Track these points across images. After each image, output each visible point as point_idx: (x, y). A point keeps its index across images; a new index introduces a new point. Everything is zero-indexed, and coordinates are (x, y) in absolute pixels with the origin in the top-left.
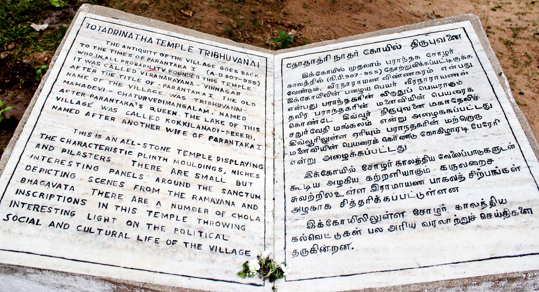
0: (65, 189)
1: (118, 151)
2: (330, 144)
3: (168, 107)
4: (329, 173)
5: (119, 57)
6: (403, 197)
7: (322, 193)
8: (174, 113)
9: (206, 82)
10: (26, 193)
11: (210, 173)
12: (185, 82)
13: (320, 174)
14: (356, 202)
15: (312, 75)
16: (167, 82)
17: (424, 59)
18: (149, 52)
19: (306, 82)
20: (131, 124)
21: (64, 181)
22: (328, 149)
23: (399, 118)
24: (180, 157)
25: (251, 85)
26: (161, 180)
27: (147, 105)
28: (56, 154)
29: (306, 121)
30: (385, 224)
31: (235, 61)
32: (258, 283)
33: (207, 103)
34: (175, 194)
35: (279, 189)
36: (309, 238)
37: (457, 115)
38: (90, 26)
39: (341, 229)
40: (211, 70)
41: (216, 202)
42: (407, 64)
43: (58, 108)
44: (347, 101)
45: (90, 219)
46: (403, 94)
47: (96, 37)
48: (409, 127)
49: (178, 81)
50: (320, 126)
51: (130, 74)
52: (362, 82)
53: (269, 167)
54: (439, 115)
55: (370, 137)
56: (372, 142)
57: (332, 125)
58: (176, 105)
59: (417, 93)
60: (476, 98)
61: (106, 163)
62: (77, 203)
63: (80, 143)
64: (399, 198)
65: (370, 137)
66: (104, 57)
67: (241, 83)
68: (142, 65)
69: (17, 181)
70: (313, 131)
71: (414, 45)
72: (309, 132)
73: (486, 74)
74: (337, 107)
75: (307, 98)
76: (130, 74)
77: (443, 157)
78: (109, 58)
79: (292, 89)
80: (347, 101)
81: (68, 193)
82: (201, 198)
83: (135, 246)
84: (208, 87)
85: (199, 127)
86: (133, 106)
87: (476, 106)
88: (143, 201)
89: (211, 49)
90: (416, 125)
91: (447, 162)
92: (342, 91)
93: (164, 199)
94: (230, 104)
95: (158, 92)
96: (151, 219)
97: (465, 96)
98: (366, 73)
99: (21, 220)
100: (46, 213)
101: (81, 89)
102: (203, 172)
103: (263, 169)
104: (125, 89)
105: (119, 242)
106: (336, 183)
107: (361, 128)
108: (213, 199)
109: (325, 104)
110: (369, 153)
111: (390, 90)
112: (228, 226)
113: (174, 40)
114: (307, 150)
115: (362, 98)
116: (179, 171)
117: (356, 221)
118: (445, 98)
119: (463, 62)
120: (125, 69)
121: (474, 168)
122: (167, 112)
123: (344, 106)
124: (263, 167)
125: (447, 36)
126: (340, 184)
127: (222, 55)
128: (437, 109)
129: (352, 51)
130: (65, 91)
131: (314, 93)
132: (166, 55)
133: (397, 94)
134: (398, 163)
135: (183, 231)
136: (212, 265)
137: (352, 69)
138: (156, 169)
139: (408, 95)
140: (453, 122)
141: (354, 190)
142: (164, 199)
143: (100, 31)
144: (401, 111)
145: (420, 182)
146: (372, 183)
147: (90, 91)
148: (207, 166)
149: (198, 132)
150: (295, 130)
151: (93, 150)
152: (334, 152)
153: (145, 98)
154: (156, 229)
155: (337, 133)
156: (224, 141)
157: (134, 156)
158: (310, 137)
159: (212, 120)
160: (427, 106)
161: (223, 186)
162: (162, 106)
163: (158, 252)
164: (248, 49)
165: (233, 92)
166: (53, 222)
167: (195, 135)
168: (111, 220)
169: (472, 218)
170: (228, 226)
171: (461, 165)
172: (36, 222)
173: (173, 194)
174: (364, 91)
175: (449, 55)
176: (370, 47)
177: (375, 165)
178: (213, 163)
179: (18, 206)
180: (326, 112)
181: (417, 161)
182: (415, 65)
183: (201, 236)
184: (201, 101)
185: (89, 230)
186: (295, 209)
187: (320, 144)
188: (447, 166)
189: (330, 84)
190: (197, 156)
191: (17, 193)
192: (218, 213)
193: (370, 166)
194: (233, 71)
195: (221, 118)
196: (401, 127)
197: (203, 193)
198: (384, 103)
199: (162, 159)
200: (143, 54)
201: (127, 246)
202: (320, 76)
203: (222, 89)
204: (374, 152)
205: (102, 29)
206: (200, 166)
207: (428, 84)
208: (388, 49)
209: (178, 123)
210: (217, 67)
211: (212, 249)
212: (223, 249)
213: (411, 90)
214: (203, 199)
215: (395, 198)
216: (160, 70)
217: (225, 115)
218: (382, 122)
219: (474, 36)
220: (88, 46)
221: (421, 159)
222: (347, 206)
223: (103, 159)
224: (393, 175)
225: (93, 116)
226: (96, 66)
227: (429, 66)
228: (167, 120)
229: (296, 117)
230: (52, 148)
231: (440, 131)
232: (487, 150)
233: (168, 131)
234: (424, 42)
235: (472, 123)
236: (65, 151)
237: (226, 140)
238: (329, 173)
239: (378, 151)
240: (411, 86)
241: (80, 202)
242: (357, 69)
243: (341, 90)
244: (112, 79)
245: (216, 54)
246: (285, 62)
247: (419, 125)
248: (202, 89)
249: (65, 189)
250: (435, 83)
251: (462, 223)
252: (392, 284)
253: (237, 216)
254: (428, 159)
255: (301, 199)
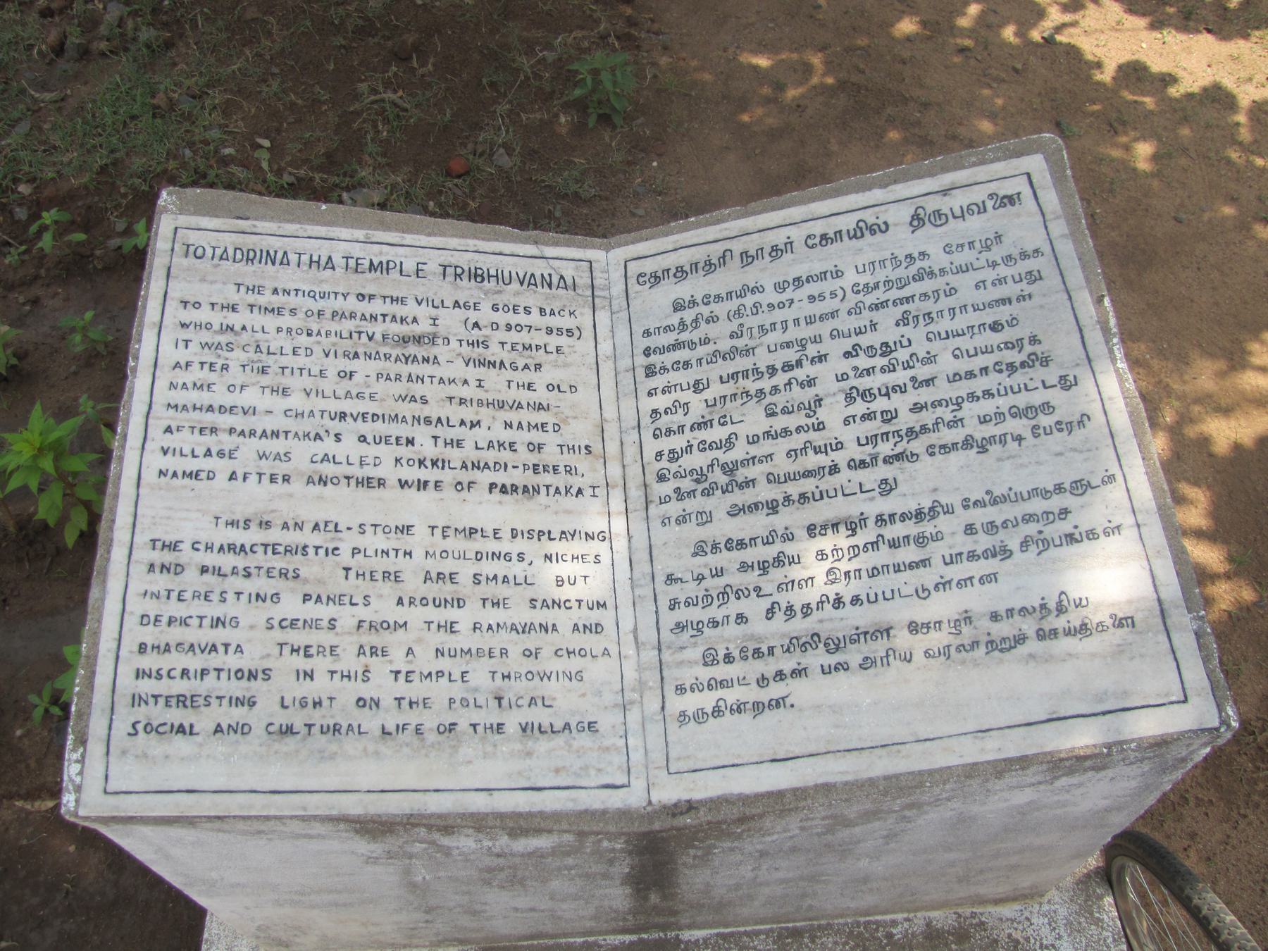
0: (226, 652)
1: (311, 551)
2: (741, 474)
3: (395, 430)
4: (741, 544)
5: (271, 322)
6: (888, 595)
7: (728, 589)
8: (410, 442)
9: (466, 350)
10: (154, 674)
11: (498, 567)
12: (420, 359)
13: (722, 546)
14: (797, 608)
15: (693, 303)
16: (380, 365)
17: (938, 259)
18: (332, 296)
19: (682, 323)
20: (325, 484)
21: (220, 635)
22: (736, 489)
23: (882, 413)
24: (439, 543)
25: (563, 341)
26: (406, 601)
27: (350, 429)
28: (191, 580)
29: (688, 421)
30: (853, 656)
31: (522, 284)
32: (618, 783)
33: (475, 404)
34: (439, 626)
35: (642, 582)
36: (709, 685)
37: (1003, 403)
38: (192, 249)
39: (768, 667)
40: (473, 316)
41: (520, 630)
42: (901, 272)
43: (170, 473)
44: (772, 370)
45: (287, 707)
46: (891, 351)
47: (210, 278)
48: (903, 433)
49: (407, 359)
50: (716, 433)
51: (301, 361)
52: (802, 322)
53: (618, 535)
54: (966, 405)
55: (822, 460)
56: (827, 470)
57: (743, 430)
58: (409, 420)
59: (921, 349)
60: (1045, 362)
61: (291, 584)
62: (255, 678)
63: (232, 548)
64: (880, 597)
65: (822, 460)
66: (238, 328)
67: (539, 338)
68: (323, 333)
69: (131, 652)
70: (704, 447)
71: (917, 221)
72: (695, 448)
73: (1070, 298)
74: (752, 385)
75: (687, 364)
76: (301, 361)
77: (971, 504)
78: (249, 328)
79: (653, 342)
80: (772, 370)
81: (233, 661)
82: (490, 627)
83: (382, 748)
84: (471, 363)
85: (464, 466)
86: (321, 439)
87: (1043, 382)
88: (379, 653)
89: (464, 260)
90: (917, 429)
91: (979, 516)
92: (761, 345)
93: (419, 641)
94: (524, 396)
95: (367, 396)
96: (402, 688)
97: (1023, 357)
98: (812, 298)
99: (161, 729)
100: (203, 708)
101: (208, 419)
102: (488, 568)
103: (607, 542)
104: (296, 401)
105: (351, 744)
106: (756, 565)
107: (803, 437)
108: (505, 576)
109: (725, 379)
110: (822, 498)
111: (865, 341)
112: (549, 678)
113: (381, 253)
114: (694, 491)
115: (804, 362)
116: (439, 574)
117: (798, 650)
118: (981, 361)
119: (1024, 266)
120: (288, 349)
121: (1031, 529)
122: (393, 440)
123: (766, 384)
124: (607, 535)
125: (991, 196)
126: (764, 567)
127: (493, 272)
128: (963, 388)
129: (779, 237)
130: (174, 428)
131: (702, 351)
132: (371, 297)
133: (879, 352)
134: (880, 520)
135: (464, 703)
136: (528, 761)
137: (780, 287)
138: (392, 577)
139: (902, 354)
140: (994, 421)
141: (793, 581)
142: (419, 641)
143: (216, 261)
144: (887, 394)
145: (924, 563)
146: (827, 565)
147: (225, 421)
148: (493, 553)
149: (465, 477)
150: (666, 444)
151: (260, 558)
152: (748, 496)
153: (343, 416)
154: (414, 706)
155: (754, 450)
156: (520, 491)
157: (345, 557)
158: (697, 460)
159: (490, 445)
160: (941, 382)
161: (530, 593)
162: (381, 428)
163: (424, 752)
164: (547, 245)
165: (526, 367)
166: (219, 725)
167: (459, 487)
168: (326, 703)
169: (1020, 639)
170: (549, 678)
171: (1005, 522)
172: (188, 730)
173: (434, 626)
174: (809, 346)
175: (994, 248)
176: (818, 228)
177: (833, 525)
178: (505, 546)
179: (146, 703)
180: (728, 399)
181: (919, 515)
182: (918, 277)
183: (500, 706)
184: (462, 402)
185: (289, 731)
186: (678, 625)
187: (719, 477)
188: (978, 526)
189: (734, 326)
190: (471, 533)
191: (137, 677)
192: (528, 654)
193: (824, 527)
194: (521, 310)
195: (507, 436)
196: (887, 434)
197: (493, 616)
198: (851, 374)
199: (401, 553)
200: (321, 304)
201: (365, 750)
202: (713, 306)
203: (502, 363)
204: (832, 493)
205: (219, 252)
206: (479, 556)
207: (944, 325)
208: (859, 234)
209: (421, 463)
210: (486, 307)
211: (524, 730)
212: (546, 726)
213: (909, 340)
214: (495, 627)
215: (872, 598)
216: (364, 336)
217: (515, 425)
218: (846, 422)
219: (1050, 198)
220: (197, 305)
221: (926, 511)
222: (780, 616)
223: (286, 575)
224: (869, 546)
225: (245, 478)
226: (225, 354)
227: (949, 278)
228: (397, 460)
229: (666, 412)
230: (179, 569)
231: (968, 443)
232: (1059, 488)
233: (402, 487)
234: (938, 213)
235: (1033, 422)
236: (207, 571)
237: (525, 486)
238: (741, 544)
239: (840, 493)
240: (907, 331)
241: (260, 675)
242: (792, 287)
243: (758, 341)
244: (265, 380)
245: (479, 272)
246: (634, 268)
247: (924, 429)
248: (458, 370)
249: (226, 652)
250: (960, 322)
251: (1001, 651)
252: (865, 775)
253: (564, 652)
254: (939, 509)
255: (687, 604)
